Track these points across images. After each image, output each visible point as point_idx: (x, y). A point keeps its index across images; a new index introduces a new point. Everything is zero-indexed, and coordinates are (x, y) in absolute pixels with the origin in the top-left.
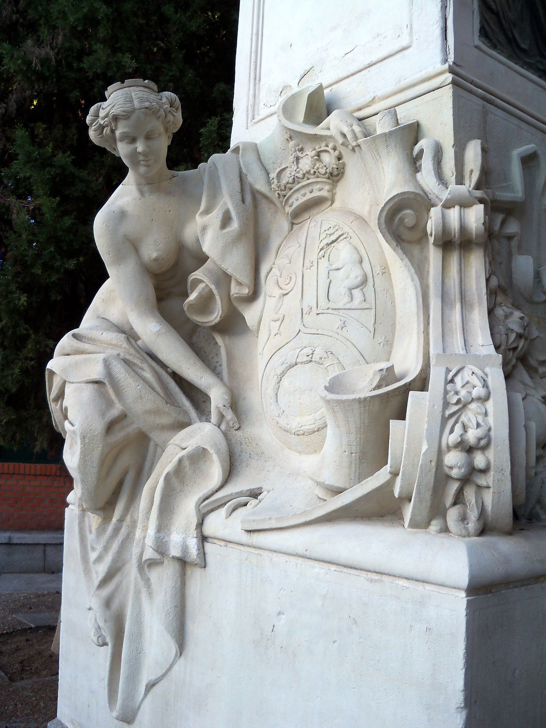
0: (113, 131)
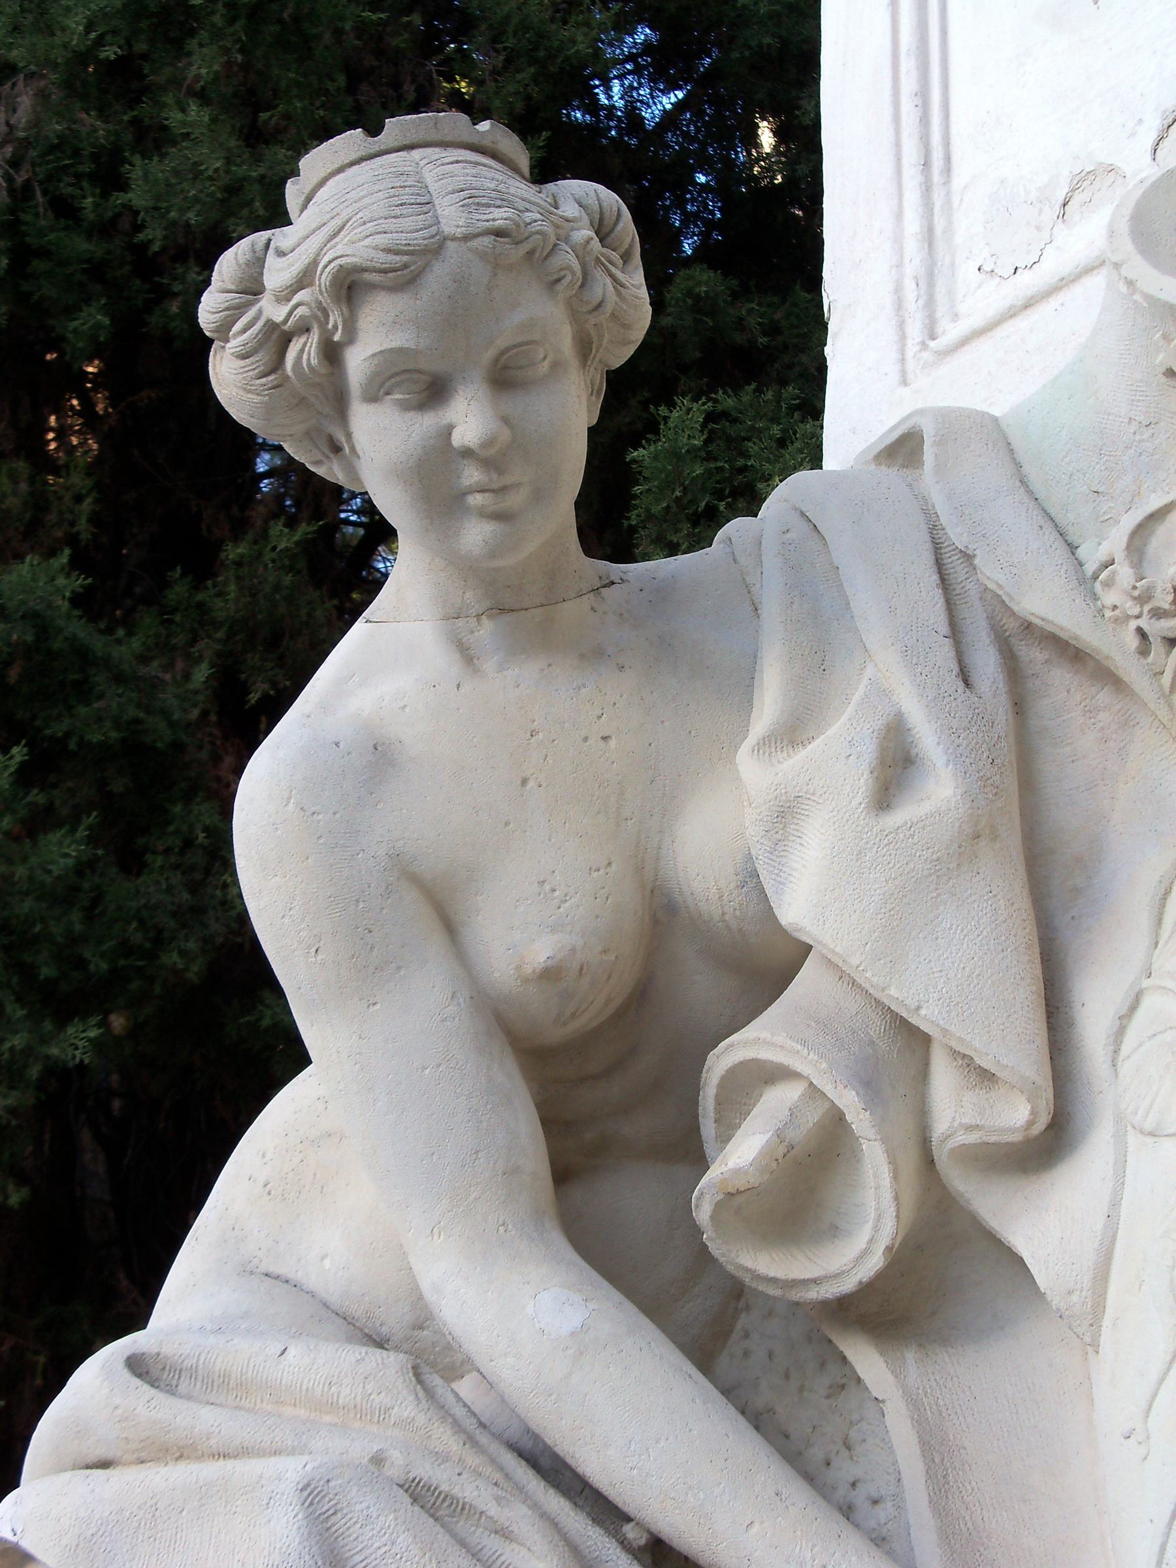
0: (332, 353)
